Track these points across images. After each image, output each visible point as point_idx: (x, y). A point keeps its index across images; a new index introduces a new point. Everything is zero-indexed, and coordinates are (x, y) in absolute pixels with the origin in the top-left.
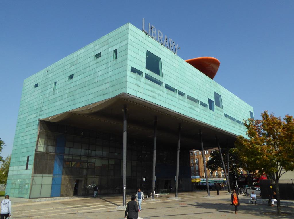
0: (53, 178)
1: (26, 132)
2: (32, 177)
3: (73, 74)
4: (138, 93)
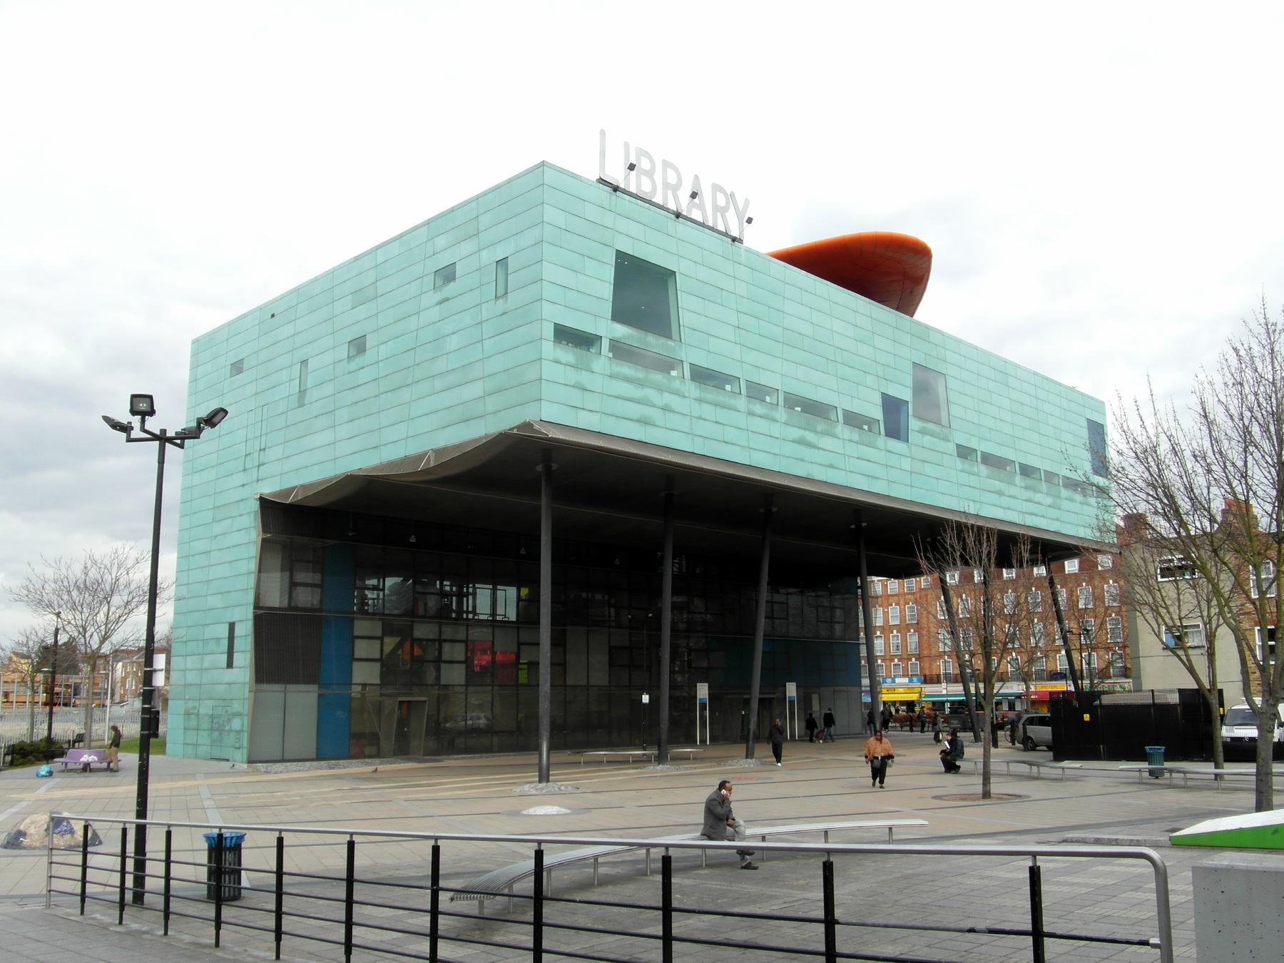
0: (320, 696)
2: (250, 692)
4: (582, 414)
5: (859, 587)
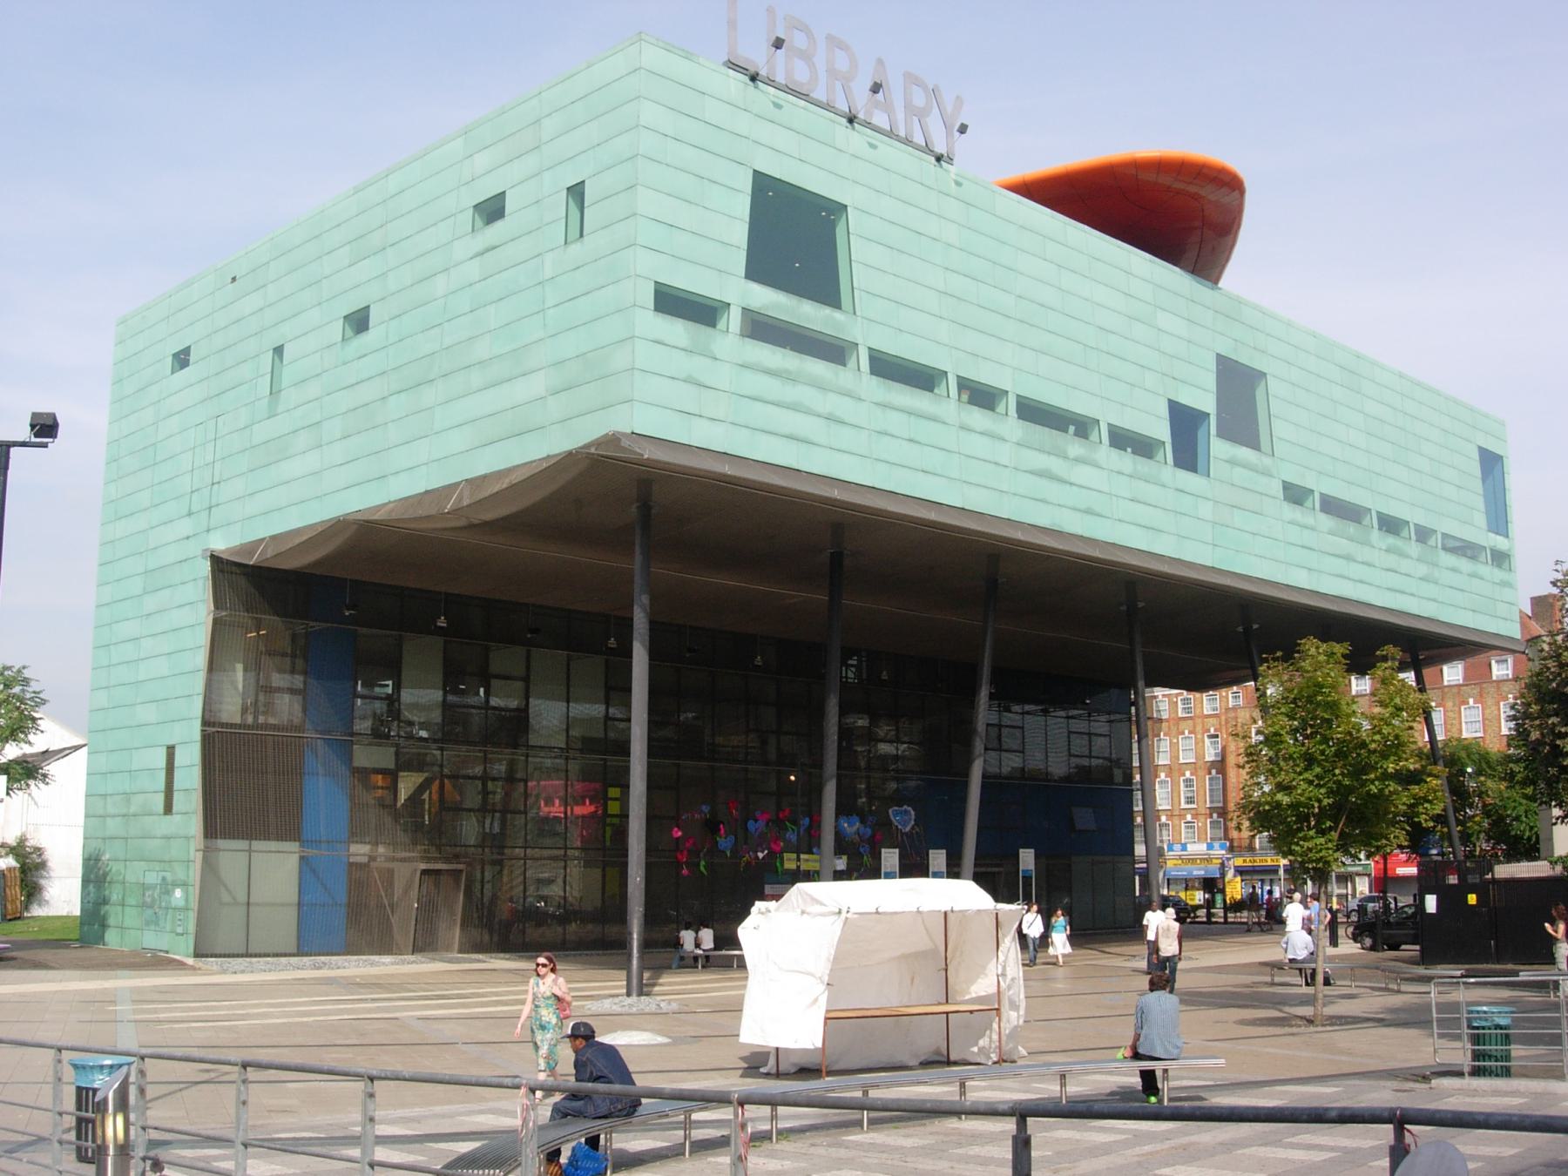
0: (302, 858)
1: (149, 615)
3: (368, 307)
5: (1133, 704)
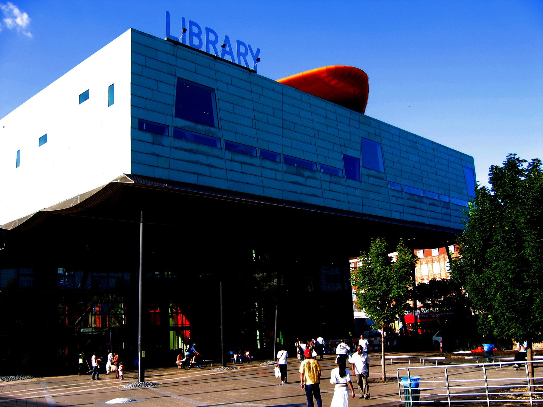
4: (157, 170)
